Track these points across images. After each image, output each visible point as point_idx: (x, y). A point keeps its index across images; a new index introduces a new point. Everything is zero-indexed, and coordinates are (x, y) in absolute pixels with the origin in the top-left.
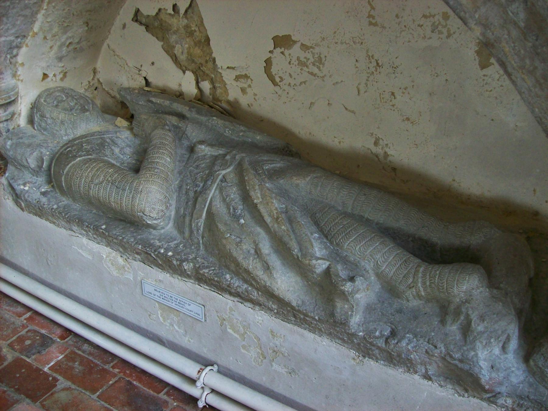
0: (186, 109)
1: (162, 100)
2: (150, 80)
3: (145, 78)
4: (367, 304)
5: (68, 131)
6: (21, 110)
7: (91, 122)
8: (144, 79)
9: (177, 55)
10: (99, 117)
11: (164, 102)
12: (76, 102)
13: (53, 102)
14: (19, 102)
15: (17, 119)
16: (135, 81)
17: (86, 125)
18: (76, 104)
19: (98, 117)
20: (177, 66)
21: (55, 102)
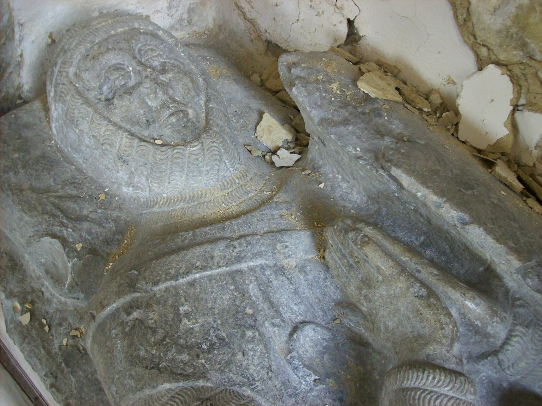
0: (508, 261)
1: (435, 198)
2: (362, 29)
3: (350, 23)
4: (360, 38)
5: (136, 179)
6: (21, 56)
7: (200, 172)
8: (345, 22)
9: (472, 7)
10: (224, 158)
11: (439, 206)
12: (165, 98)
13: (101, 88)
14: (17, 37)
15: (14, 76)
16: (318, 15)
17: (187, 178)
18: (164, 106)
19: (221, 160)
20: (463, 36)
21: (105, 88)
